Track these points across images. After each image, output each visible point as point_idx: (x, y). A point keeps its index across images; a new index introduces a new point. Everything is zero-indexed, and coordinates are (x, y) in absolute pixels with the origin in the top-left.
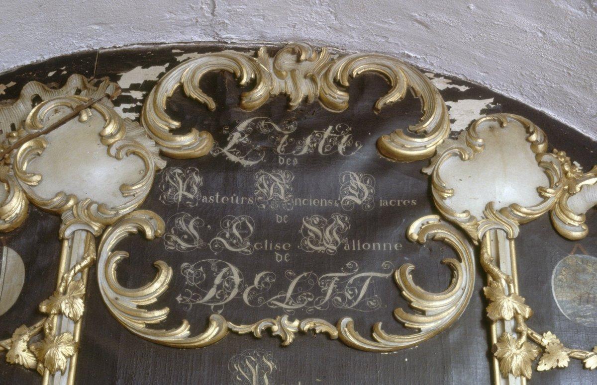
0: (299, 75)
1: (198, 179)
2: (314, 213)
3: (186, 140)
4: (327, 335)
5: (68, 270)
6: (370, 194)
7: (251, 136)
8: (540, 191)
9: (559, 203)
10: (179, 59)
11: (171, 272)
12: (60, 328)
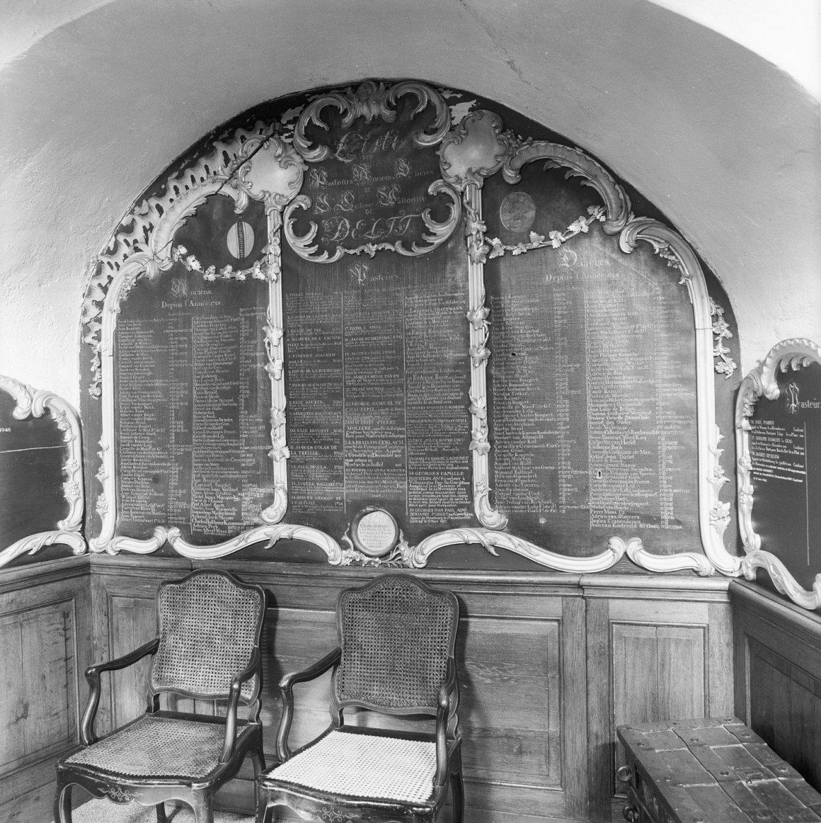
1: (325, 173)
2: (382, 185)
3: (317, 152)
6: (410, 170)
7: (348, 143)
10: (309, 100)
11: (317, 226)
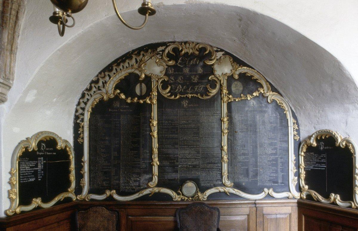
0: (190, 48)
1: (173, 69)
4: (196, 96)
5: (154, 87)
8: (231, 70)
9: (234, 73)
12: (154, 97)
